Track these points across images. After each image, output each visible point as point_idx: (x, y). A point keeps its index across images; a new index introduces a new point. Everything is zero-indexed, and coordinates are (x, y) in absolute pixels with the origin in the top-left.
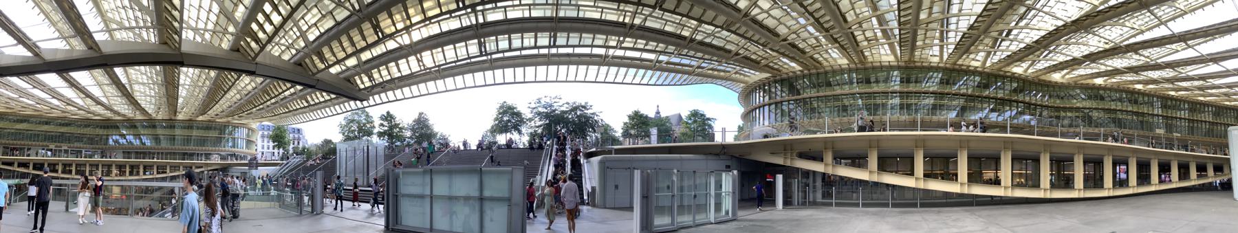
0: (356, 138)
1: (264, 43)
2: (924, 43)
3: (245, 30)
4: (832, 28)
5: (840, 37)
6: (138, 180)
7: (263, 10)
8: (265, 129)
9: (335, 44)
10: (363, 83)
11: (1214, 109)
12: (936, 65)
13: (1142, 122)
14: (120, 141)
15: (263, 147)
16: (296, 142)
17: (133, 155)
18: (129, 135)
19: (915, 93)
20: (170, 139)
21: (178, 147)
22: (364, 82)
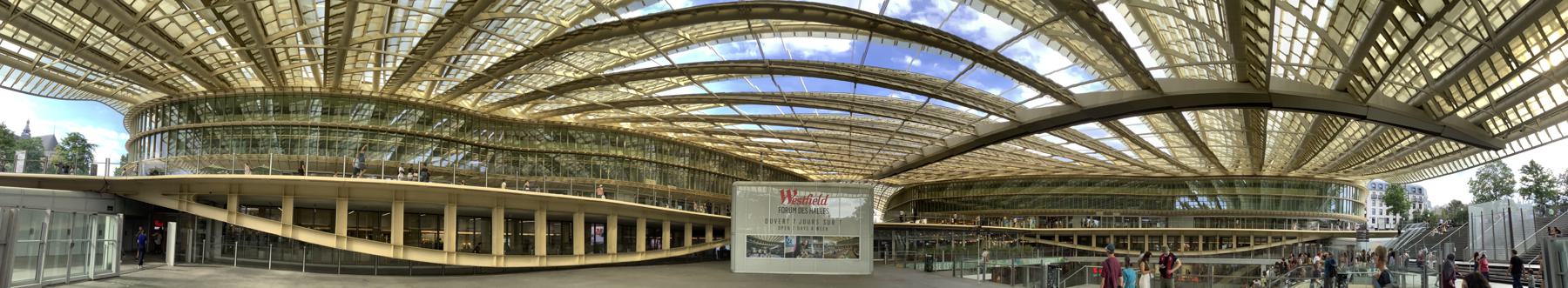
0: (1492, 198)
1: (1377, 82)
2: (355, 67)
3: (1355, 66)
4: (250, 41)
5: (258, 53)
6: (1214, 256)
7: (1376, 42)
8: (1377, 188)
9: (1463, 83)
10: (1497, 127)
11: (722, 158)
12: (368, 94)
13: (627, 170)
14: (1191, 204)
15: (1374, 212)
16: (1417, 205)
17: (1208, 223)
18: (1203, 196)
19: (340, 128)
20: (1254, 201)
21: (1264, 210)
22: (1497, 126)
